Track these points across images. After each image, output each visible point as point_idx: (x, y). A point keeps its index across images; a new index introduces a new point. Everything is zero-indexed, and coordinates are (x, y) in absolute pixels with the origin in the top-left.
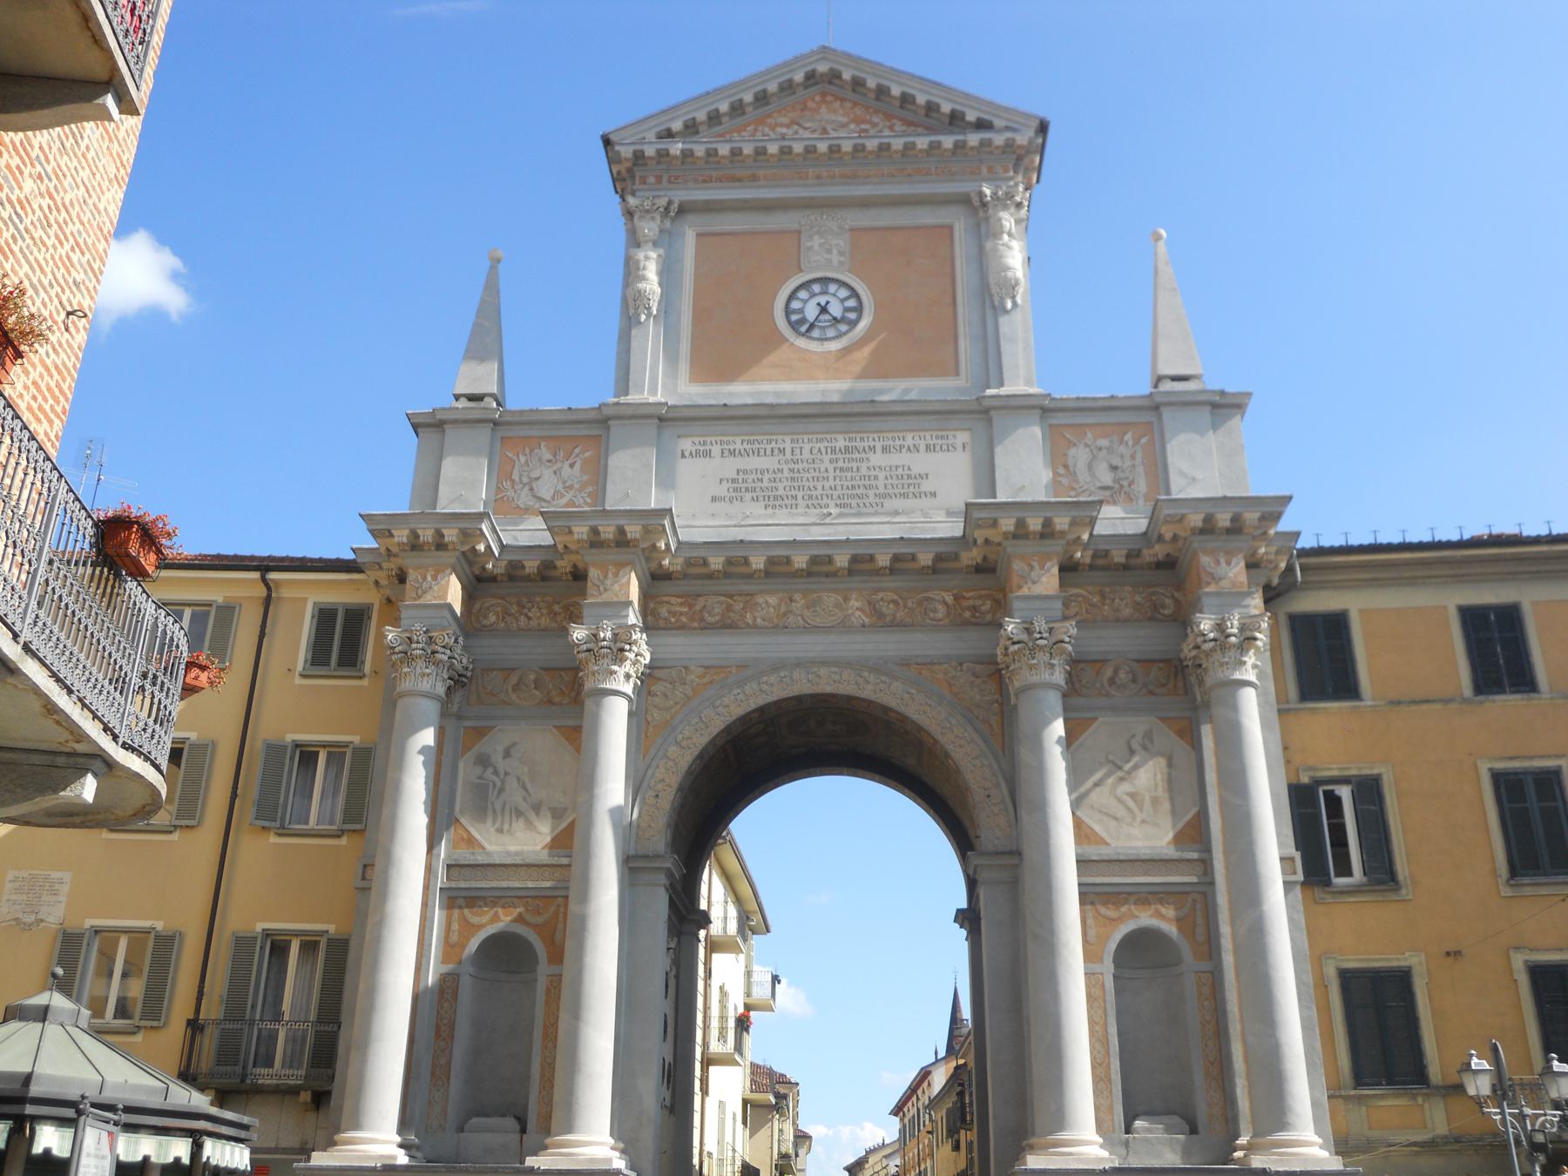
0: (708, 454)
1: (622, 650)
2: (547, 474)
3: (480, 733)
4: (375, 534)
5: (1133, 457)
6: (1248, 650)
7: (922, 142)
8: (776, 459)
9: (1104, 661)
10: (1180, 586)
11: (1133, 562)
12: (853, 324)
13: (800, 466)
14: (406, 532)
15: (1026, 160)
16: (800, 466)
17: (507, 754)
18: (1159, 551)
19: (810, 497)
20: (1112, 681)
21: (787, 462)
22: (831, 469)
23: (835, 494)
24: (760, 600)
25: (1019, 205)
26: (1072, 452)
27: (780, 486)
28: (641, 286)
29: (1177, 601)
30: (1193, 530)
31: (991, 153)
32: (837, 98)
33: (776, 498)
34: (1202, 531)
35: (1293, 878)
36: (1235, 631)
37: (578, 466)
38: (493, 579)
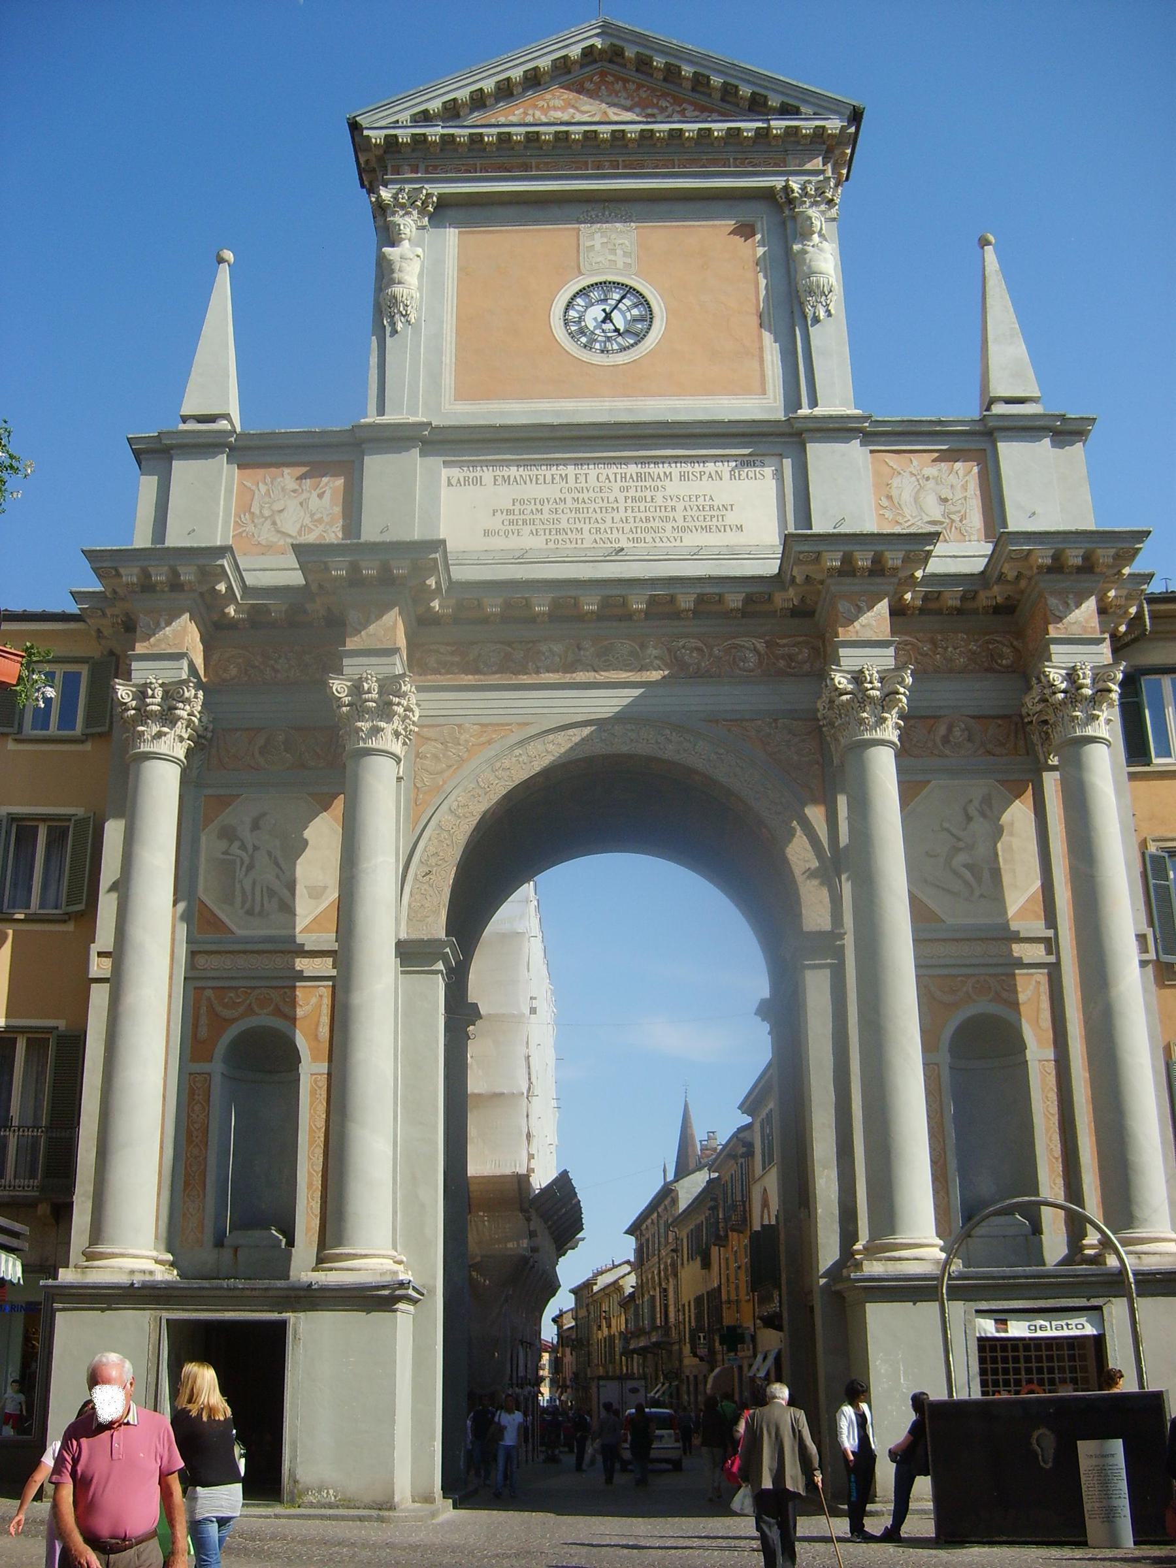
0: (478, 481)
1: (391, 704)
2: (292, 505)
3: (223, 802)
4: (99, 573)
5: (965, 488)
6: (1101, 704)
7: (719, 128)
8: (557, 487)
9: (936, 718)
10: (1020, 634)
11: (970, 605)
12: (640, 337)
13: (586, 495)
14: (136, 570)
15: (837, 152)
16: (586, 495)
17: (255, 826)
18: (998, 593)
19: (598, 531)
20: (946, 740)
21: (570, 490)
22: (621, 500)
23: (627, 527)
24: (544, 648)
25: (830, 202)
26: (896, 482)
27: (564, 518)
28: (397, 290)
29: (1016, 650)
30: (1040, 567)
31: (798, 143)
32: (618, 79)
33: (558, 531)
34: (1050, 570)
35: (1146, 957)
36: (1088, 681)
37: (327, 496)
38: (232, 625)
